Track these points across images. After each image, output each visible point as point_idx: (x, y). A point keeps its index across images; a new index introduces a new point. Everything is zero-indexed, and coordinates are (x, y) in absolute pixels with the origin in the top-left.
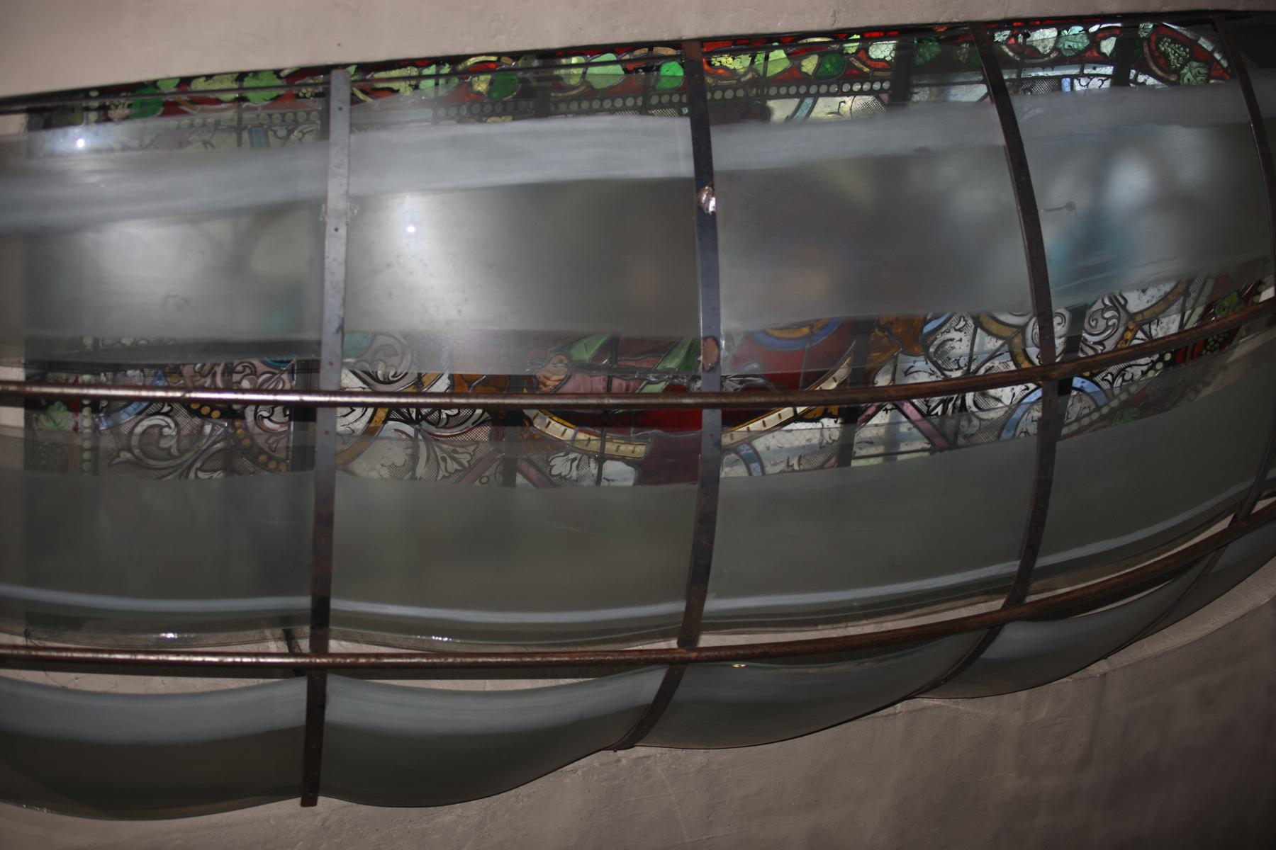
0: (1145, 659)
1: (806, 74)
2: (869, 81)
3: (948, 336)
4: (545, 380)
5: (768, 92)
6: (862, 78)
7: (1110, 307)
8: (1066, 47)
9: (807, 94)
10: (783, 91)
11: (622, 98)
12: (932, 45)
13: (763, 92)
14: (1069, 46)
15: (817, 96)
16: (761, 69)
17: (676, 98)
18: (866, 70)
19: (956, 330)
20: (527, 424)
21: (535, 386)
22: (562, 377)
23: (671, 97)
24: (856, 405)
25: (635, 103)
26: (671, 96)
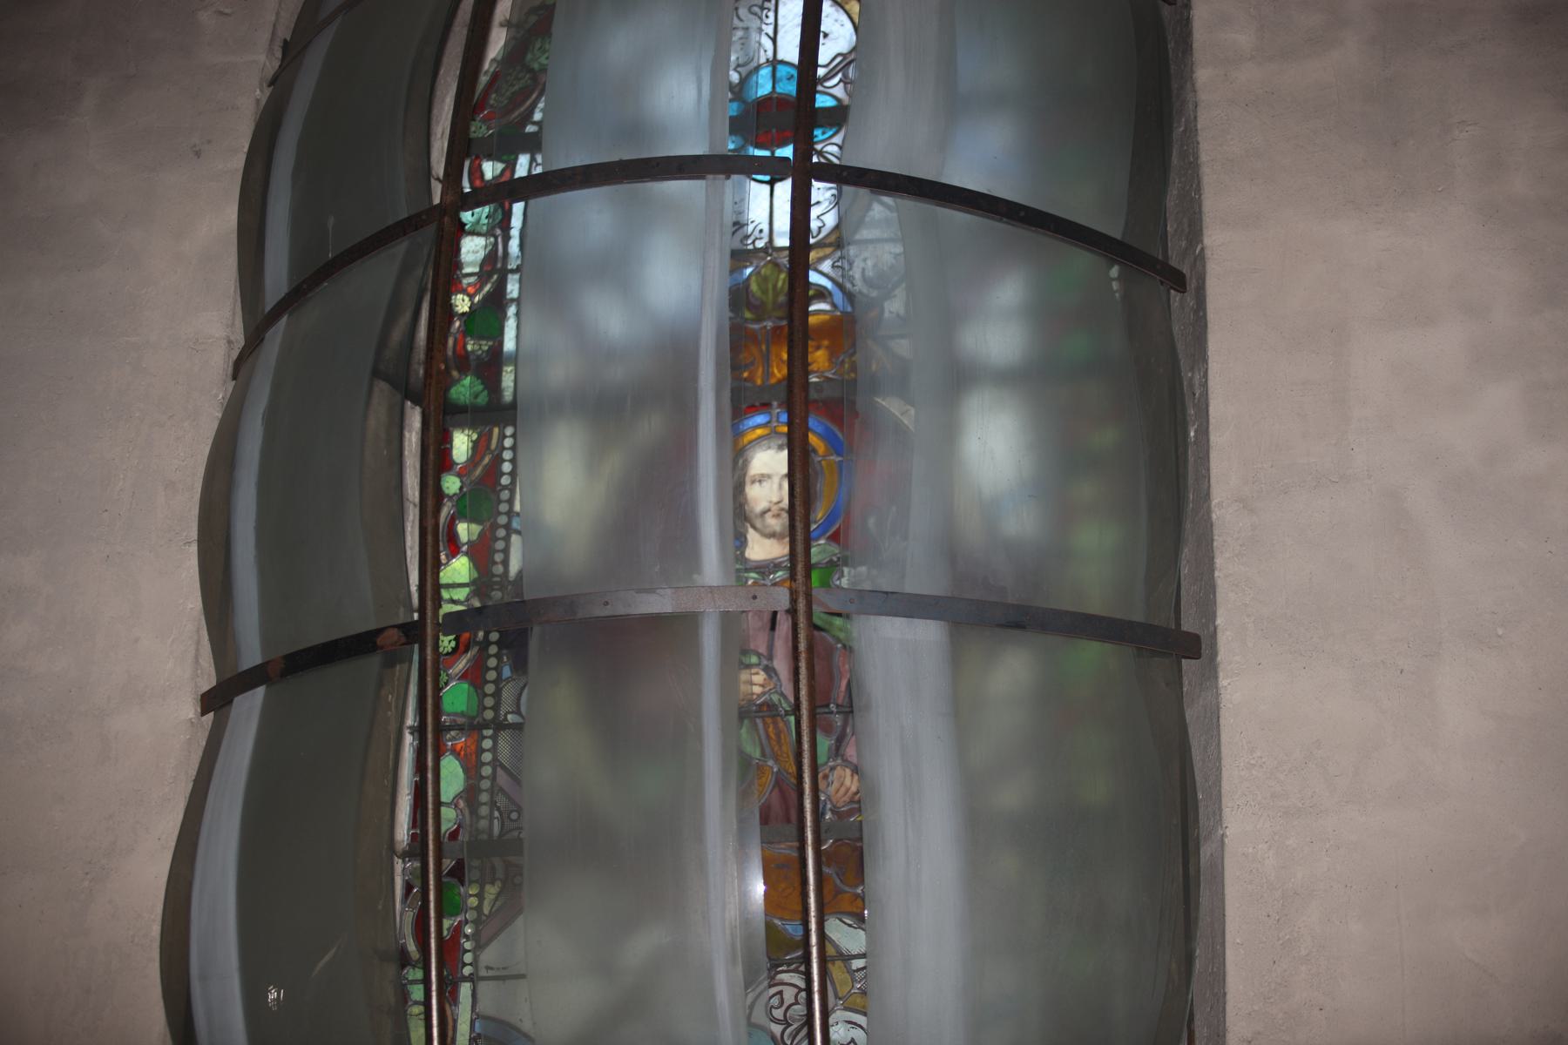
0: (1196, 107)
1: (488, 160)
2: (502, 452)
3: (858, 276)
4: (850, 793)
5: (497, 576)
6: (494, 471)
7: (843, 75)
8: (486, 221)
9: (507, 527)
10: (498, 557)
11: (499, 504)
12: (474, 964)
13: (496, 583)
14: (487, 217)
15: (510, 513)
16: (466, 591)
17: (490, 689)
18: (486, 460)
19: (851, 269)
20: (515, 834)
21: (856, 806)
22: (848, 772)
23: (505, 513)
24: (465, 846)
25: (490, 737)
26: (486, 695)
